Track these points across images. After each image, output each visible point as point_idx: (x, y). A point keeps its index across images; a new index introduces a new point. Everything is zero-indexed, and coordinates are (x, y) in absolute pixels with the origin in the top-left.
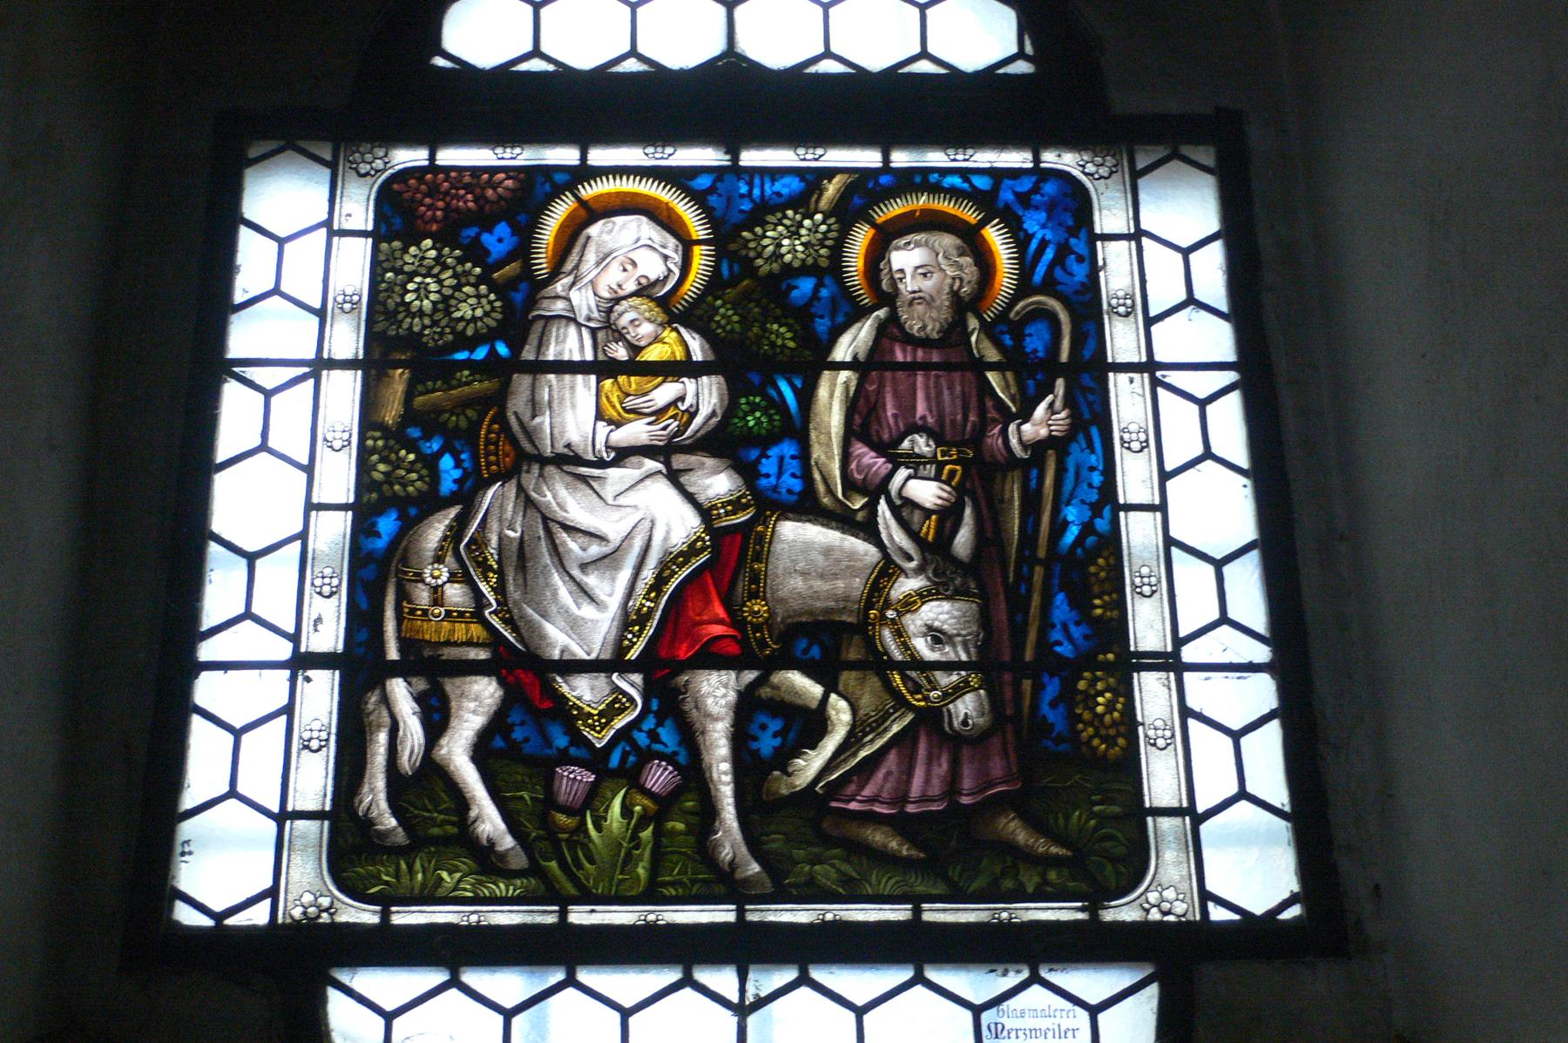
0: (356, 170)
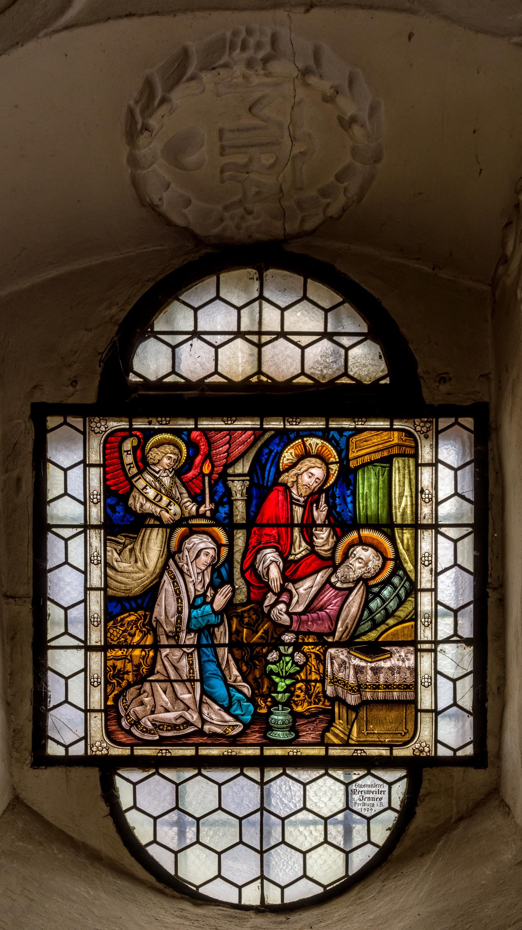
0: (94, 431)
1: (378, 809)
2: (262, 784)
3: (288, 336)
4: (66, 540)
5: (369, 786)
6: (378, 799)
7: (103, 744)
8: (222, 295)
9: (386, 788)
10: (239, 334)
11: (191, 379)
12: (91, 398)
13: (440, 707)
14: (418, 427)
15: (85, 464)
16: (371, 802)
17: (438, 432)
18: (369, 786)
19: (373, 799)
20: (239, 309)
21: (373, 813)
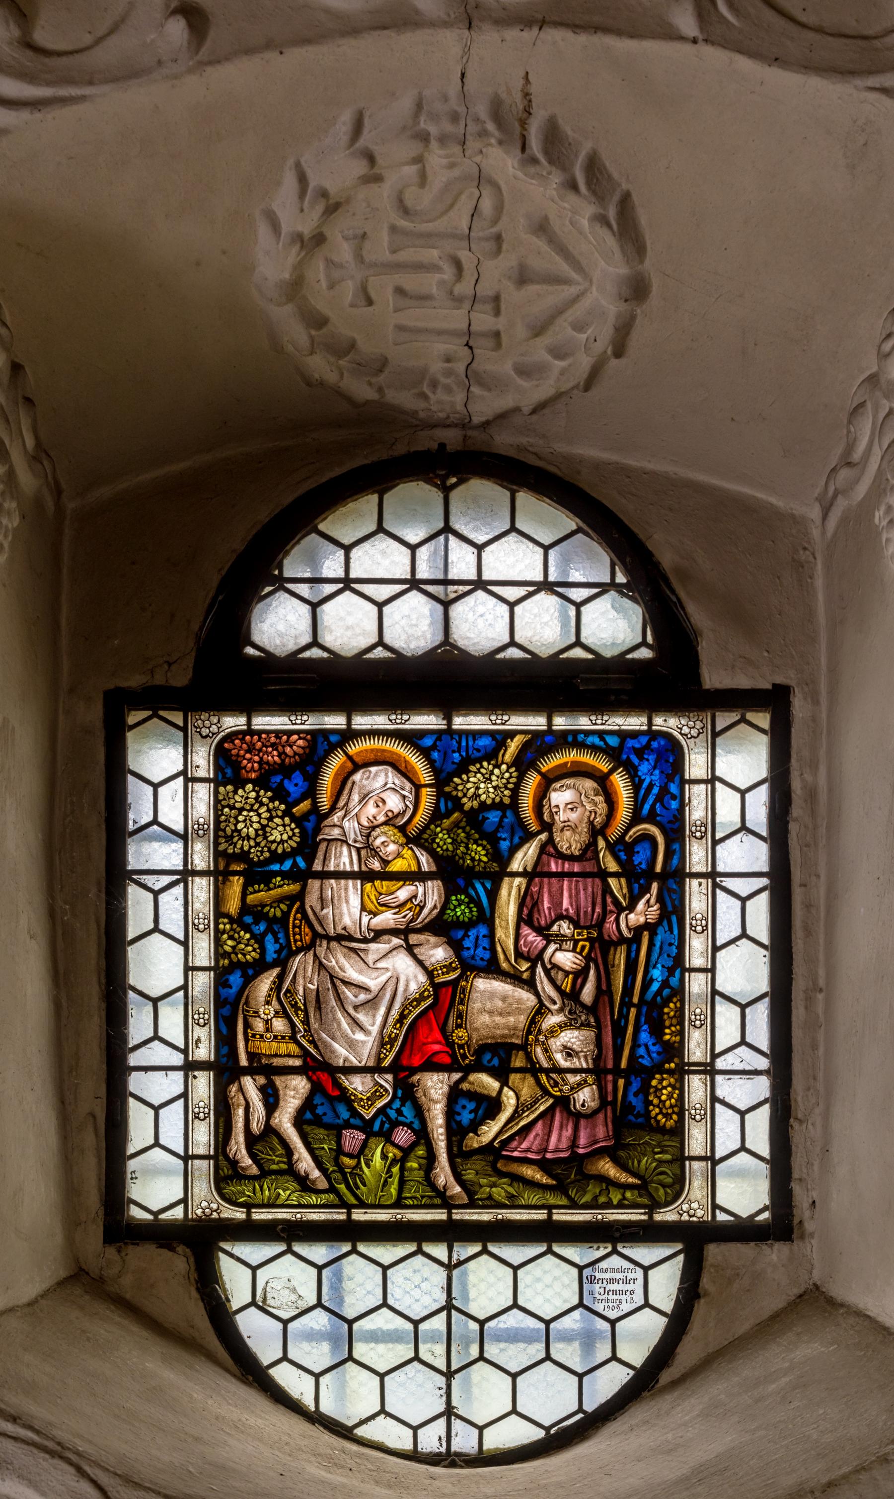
1: (626, 1308)
2: (450, 1267)
3: (489, 587)
4: (156, 894)
5: (613, 1270)
6: (628, 1293)
7: (212, 1205)
8: (518, 525)
9: (640, 1273)
10: (414, 584)
11: (540, 655)
12: (181, 677)
13: (718, 1155)
14: (214, 726)
15: (187, 777)
16: (618, 1297)
17: (715, 735)
18: (613, 1270)
19: (621, 1292)
20: (546, 549)
21: (621, 1314)
